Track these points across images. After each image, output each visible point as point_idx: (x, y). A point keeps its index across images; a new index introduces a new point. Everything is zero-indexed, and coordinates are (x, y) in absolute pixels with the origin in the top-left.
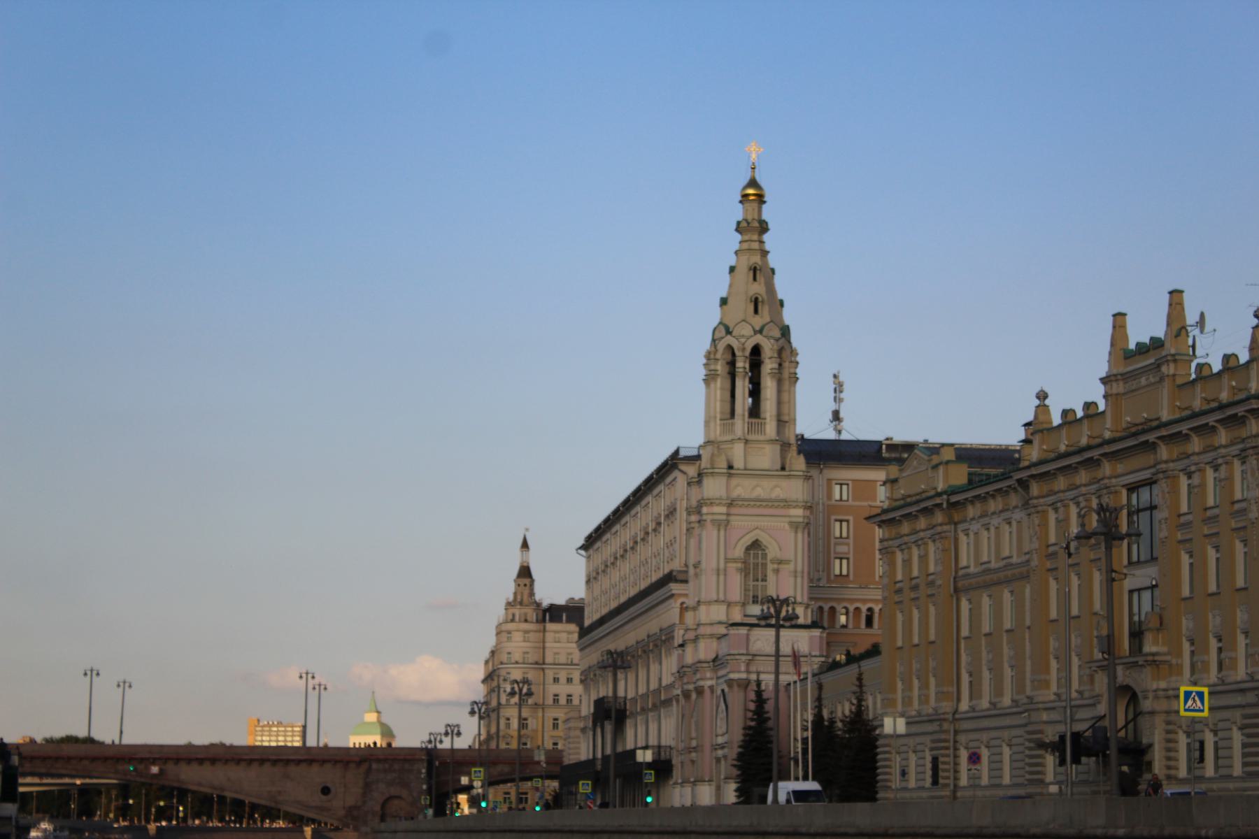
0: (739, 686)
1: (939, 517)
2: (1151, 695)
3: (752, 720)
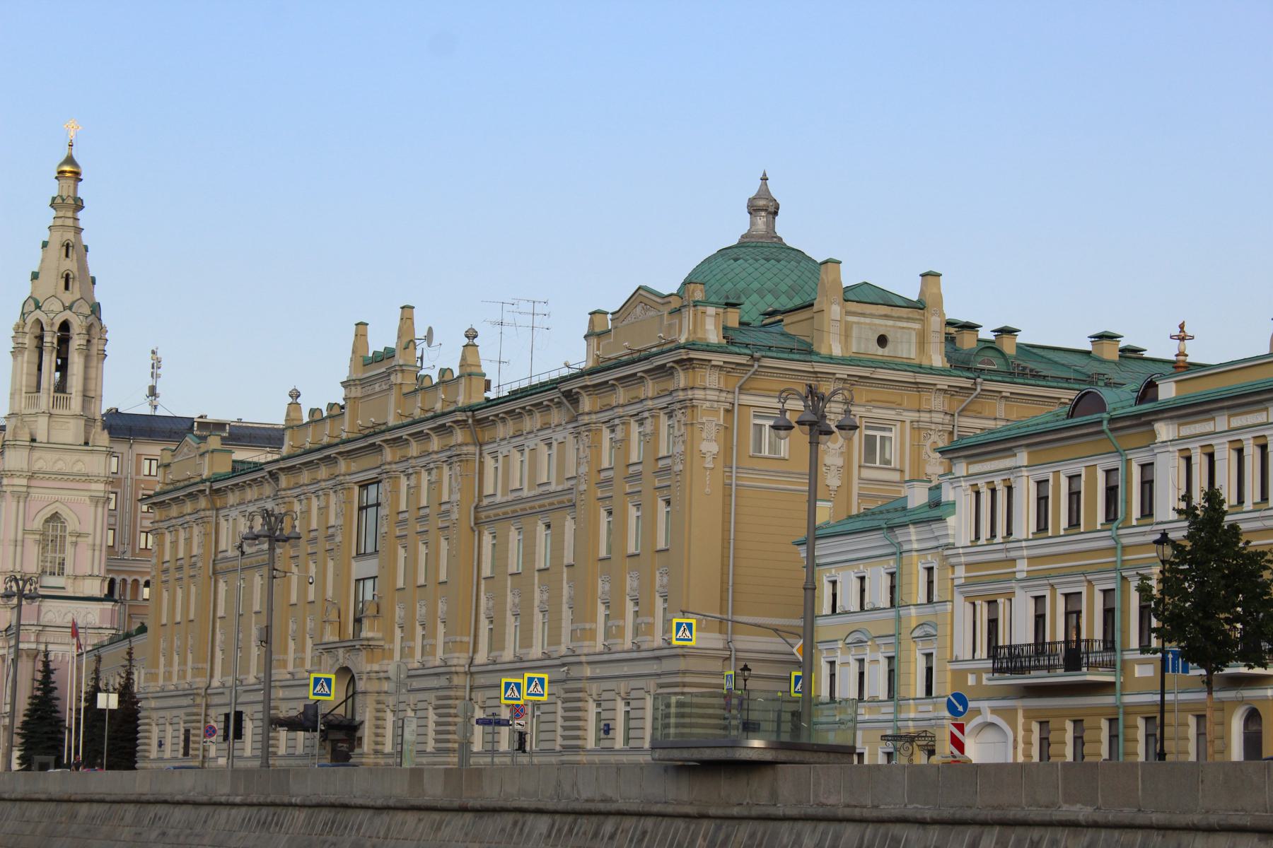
0: (28, 656)
1: (203, 503)
2: (365, 677)
3: (38, 689)
